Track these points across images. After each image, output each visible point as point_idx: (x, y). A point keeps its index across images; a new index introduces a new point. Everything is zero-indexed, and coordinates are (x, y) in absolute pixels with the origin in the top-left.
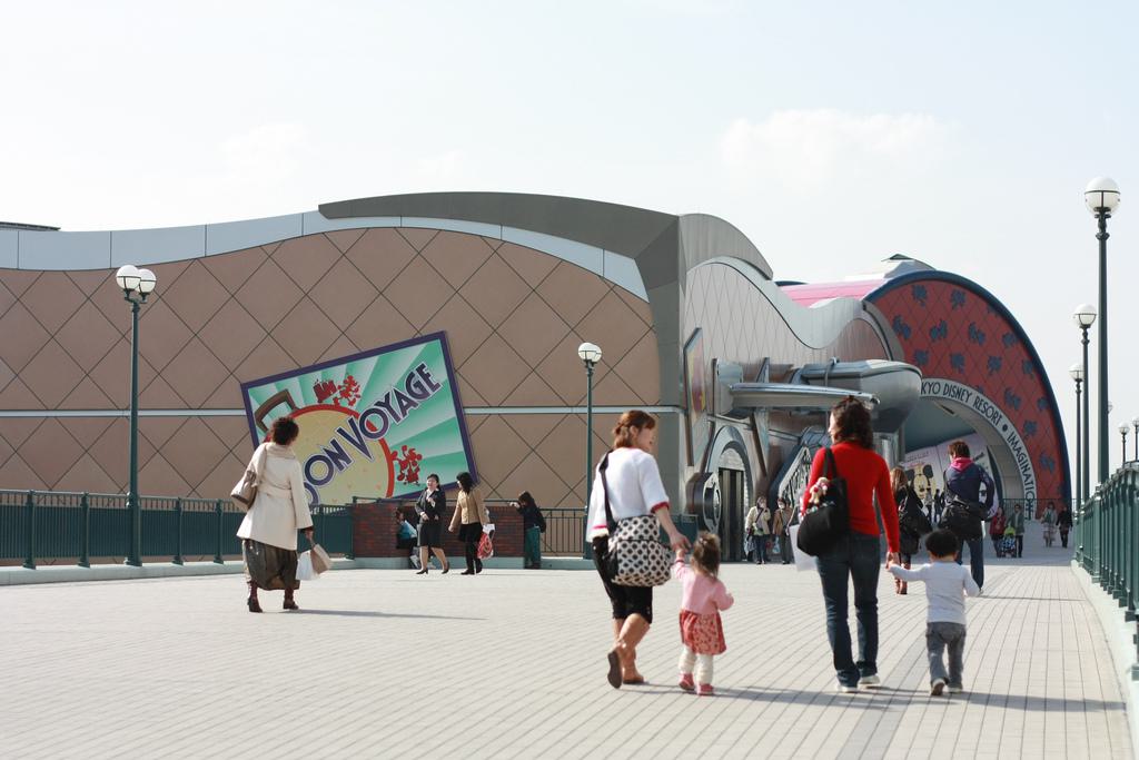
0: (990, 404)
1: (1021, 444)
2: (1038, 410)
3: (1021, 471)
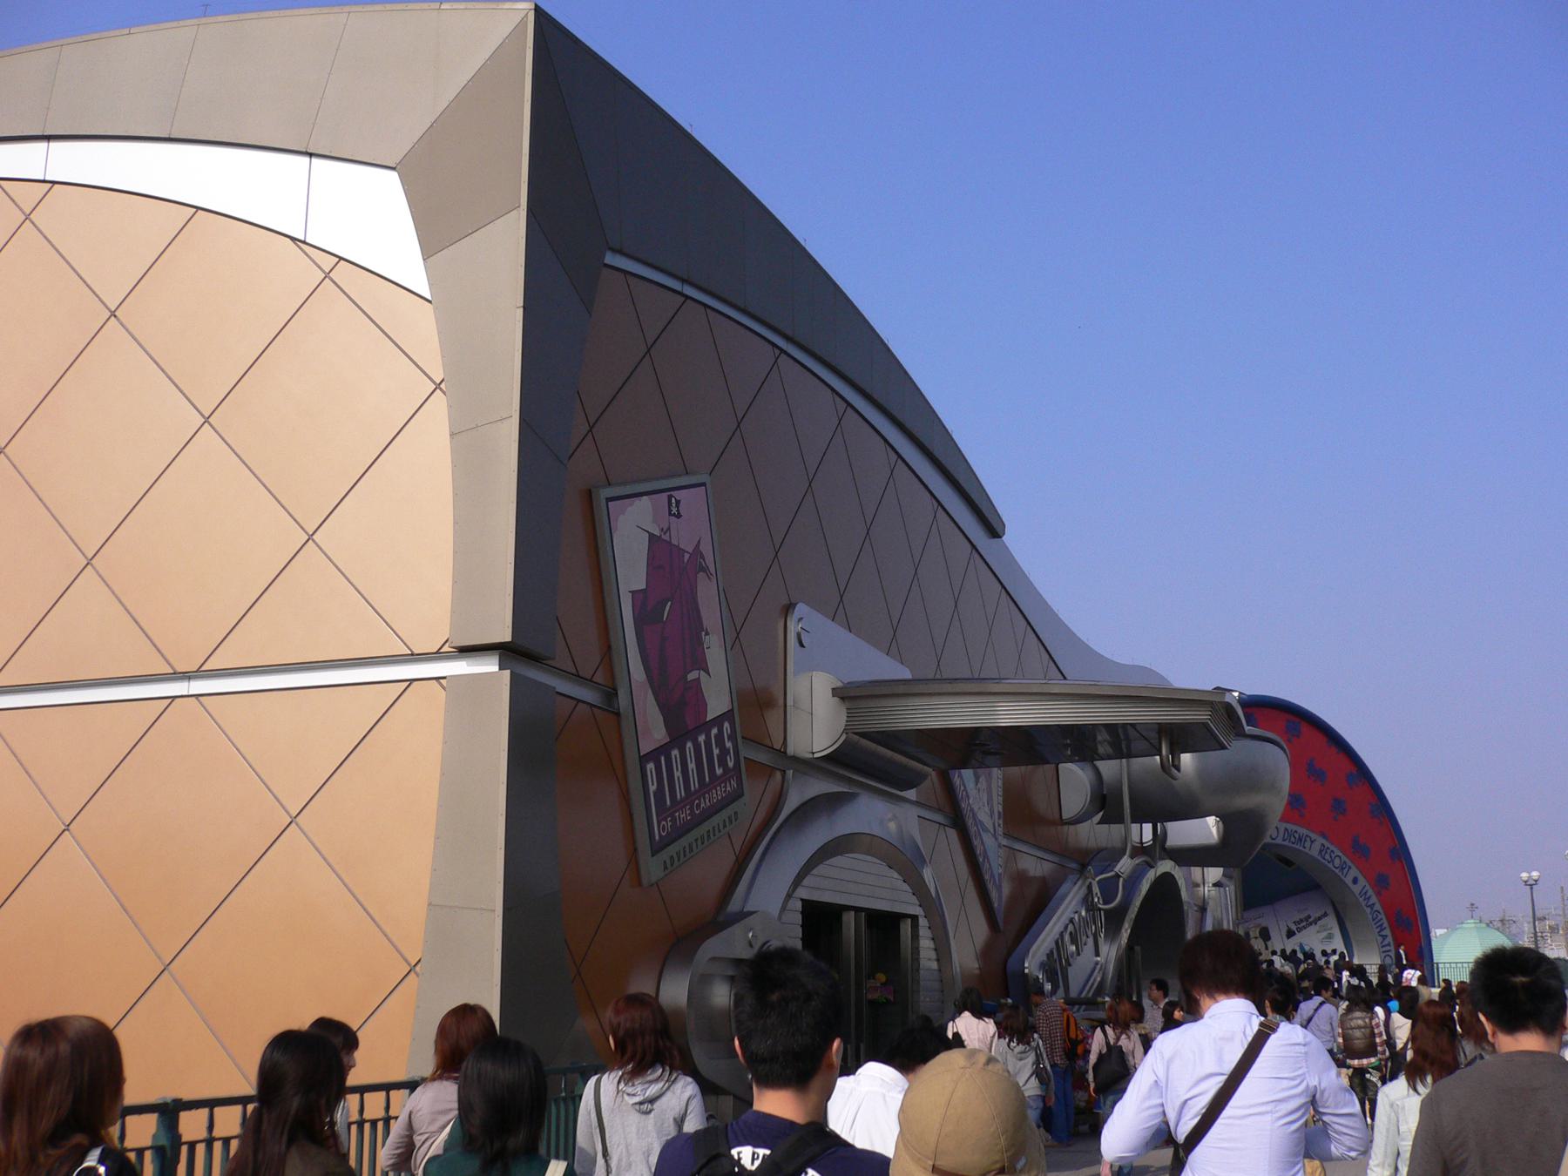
1: (1374, 899)
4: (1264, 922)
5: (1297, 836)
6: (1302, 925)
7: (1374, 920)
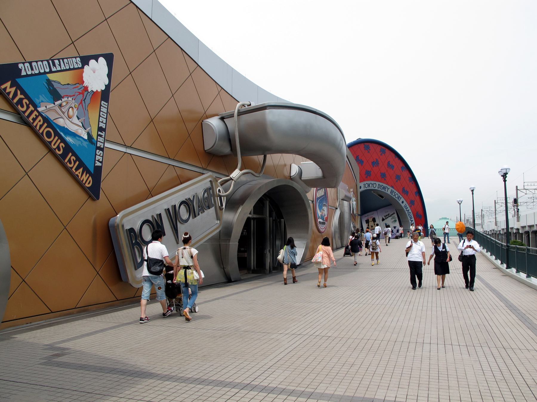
0: (397, 193)
1: (409, 208)
2: (415, 196)
3: (409, 219)
7: (408, 215)
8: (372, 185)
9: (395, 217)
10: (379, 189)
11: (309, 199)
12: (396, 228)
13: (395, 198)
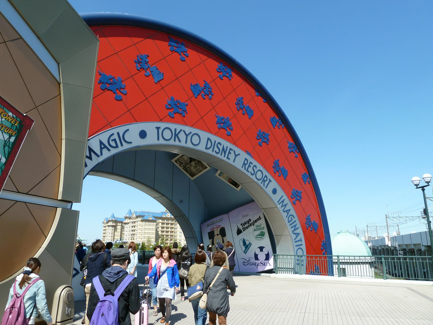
0: (260, 167)
1: (290, 206)
4: (222, 224)
5: (221, 148)
6: (246, 226)
7: (289, 222)
8: (187, 135)
9: (262, 226)
10: (210, 151)
11: (229, 213)
12: (264, 249)
13: (256, 180)
